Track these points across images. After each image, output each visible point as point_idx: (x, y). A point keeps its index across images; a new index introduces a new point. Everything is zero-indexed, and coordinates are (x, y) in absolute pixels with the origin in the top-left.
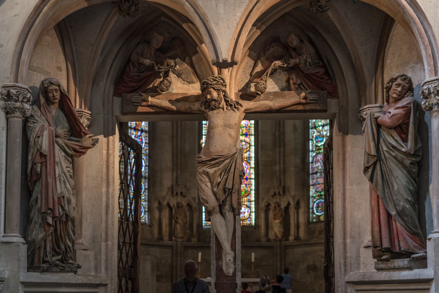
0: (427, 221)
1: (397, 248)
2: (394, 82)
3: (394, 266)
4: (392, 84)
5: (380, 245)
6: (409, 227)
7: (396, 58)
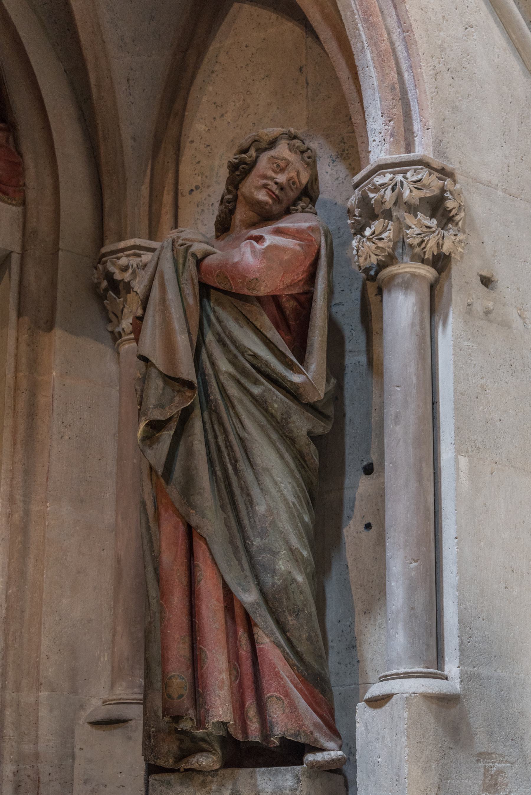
1: (254, 727)
4: (257, 157)
7: (229, 117)
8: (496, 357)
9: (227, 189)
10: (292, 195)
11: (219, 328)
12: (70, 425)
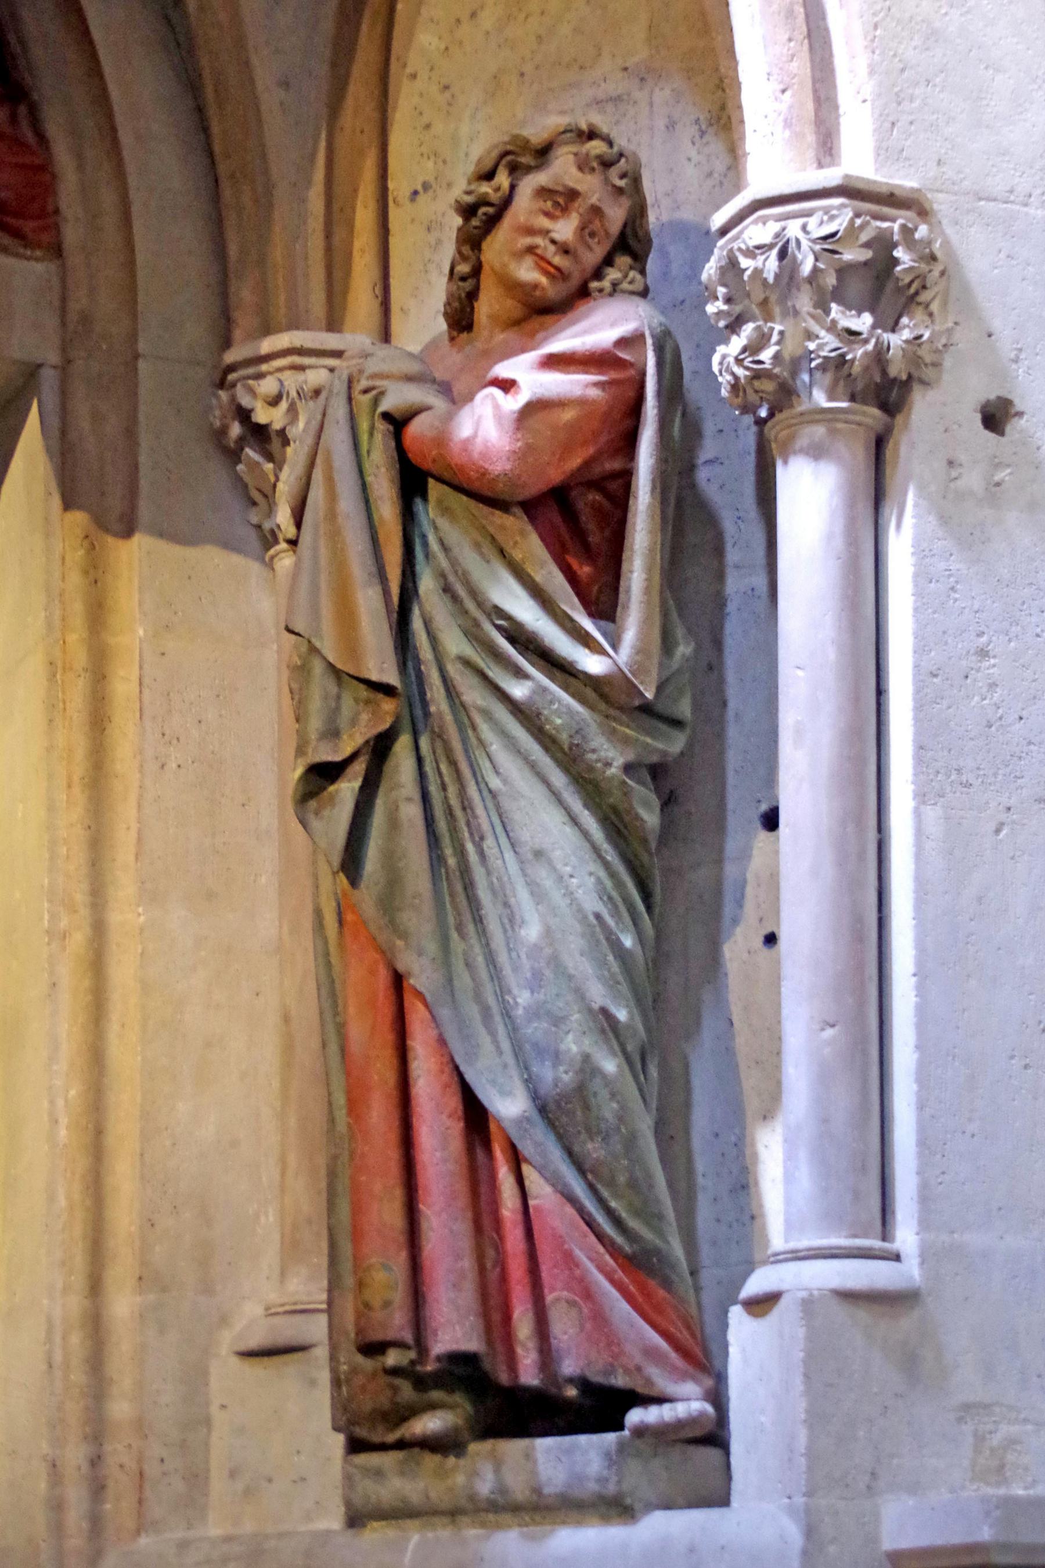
0: (700, 1180)
2: (529, 169)
3: (502, 1489)
4: (513, 187)
5: (408, 1337)
6: (610, 1213)
8: (1013, 586)
9: (460, 252)
10: (592, 257)
11: (444, 563)
12: (178, 739)
